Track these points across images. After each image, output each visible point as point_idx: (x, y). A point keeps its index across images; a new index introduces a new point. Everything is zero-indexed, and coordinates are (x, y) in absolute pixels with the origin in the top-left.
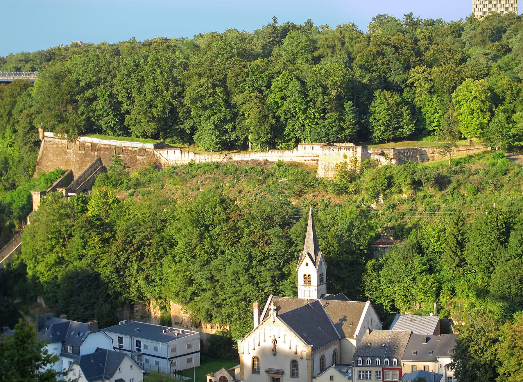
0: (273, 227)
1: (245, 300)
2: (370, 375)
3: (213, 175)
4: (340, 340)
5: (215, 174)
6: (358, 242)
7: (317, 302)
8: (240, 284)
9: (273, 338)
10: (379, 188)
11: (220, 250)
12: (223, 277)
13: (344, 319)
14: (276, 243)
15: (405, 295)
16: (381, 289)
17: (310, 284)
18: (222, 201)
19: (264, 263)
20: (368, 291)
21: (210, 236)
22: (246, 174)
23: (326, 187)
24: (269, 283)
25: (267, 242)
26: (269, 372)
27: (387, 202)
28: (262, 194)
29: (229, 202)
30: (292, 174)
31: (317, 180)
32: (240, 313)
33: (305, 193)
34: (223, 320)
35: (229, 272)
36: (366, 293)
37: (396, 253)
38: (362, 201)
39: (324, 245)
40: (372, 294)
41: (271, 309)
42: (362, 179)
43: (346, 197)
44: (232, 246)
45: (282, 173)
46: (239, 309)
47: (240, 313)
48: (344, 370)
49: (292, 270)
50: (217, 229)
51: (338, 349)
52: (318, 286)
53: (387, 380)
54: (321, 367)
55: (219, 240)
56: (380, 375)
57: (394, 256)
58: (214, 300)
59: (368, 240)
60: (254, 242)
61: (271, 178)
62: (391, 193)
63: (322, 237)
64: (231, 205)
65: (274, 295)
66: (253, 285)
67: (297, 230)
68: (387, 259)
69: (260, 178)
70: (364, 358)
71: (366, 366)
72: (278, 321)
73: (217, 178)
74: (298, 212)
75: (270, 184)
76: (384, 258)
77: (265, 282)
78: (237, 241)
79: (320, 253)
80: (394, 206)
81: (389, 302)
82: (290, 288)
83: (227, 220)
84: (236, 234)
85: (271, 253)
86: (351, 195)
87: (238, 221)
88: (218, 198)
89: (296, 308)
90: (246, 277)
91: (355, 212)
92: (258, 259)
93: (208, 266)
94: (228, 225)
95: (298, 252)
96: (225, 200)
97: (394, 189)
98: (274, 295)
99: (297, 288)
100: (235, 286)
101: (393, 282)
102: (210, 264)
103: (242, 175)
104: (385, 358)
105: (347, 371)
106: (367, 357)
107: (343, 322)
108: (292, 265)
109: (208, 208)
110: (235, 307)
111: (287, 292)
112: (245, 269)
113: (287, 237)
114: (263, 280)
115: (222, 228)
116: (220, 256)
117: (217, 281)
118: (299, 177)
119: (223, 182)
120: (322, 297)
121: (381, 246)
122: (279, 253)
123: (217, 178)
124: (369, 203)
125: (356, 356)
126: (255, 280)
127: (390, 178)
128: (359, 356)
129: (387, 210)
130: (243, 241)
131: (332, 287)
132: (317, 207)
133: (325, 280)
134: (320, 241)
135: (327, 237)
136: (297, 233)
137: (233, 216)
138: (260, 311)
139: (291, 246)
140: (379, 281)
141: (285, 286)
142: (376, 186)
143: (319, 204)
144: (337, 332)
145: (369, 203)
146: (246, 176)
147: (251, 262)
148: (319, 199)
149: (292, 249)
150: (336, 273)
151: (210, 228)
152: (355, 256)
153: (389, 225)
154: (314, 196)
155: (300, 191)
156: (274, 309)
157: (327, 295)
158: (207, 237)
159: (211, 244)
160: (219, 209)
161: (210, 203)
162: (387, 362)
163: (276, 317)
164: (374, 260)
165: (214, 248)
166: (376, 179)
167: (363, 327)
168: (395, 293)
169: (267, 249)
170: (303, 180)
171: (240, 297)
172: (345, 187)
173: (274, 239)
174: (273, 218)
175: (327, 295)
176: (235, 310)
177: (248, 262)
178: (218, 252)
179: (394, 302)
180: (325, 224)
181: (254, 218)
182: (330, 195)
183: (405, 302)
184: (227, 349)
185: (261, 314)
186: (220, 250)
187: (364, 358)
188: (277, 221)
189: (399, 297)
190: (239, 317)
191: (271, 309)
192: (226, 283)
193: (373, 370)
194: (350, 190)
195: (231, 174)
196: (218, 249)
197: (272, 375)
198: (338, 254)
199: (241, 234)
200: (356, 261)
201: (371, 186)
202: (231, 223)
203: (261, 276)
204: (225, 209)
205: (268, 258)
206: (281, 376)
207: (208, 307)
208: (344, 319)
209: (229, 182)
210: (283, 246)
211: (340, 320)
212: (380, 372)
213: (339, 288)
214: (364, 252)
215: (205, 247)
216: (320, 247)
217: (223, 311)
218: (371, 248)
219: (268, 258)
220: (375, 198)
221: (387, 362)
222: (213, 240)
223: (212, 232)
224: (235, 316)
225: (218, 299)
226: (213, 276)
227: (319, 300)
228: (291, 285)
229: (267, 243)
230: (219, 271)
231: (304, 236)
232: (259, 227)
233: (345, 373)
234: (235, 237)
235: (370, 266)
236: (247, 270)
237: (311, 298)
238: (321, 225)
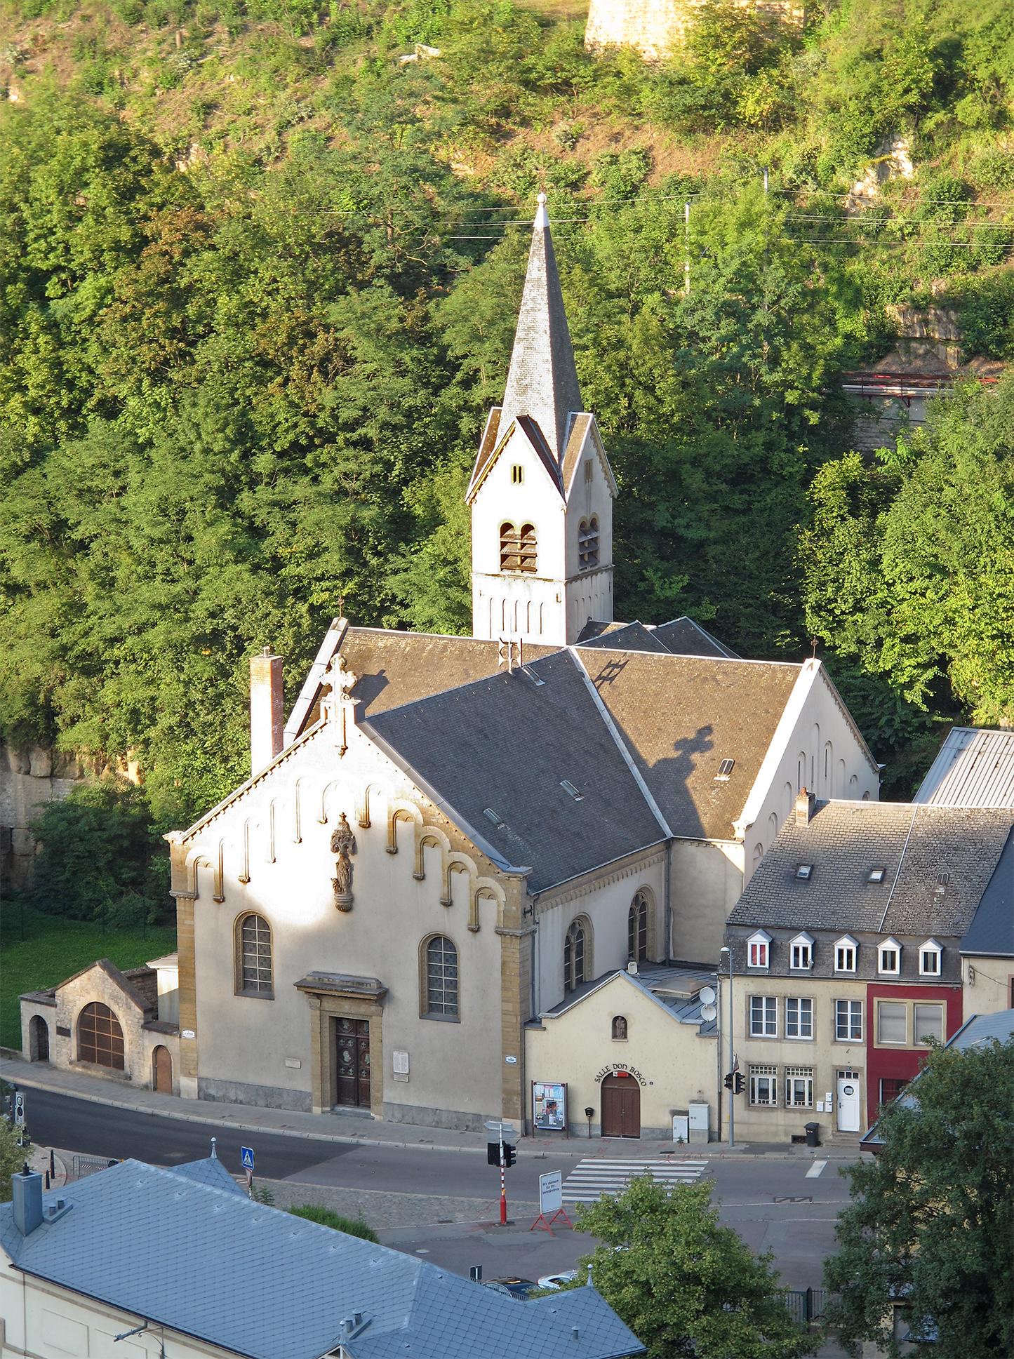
0: (362, 285)
1: (215, 638)
2: (806, 1017)
3: (76, 23)
4: (669, 844)
5: (86, 19)
6: (772, 370)
7: (563, 657)
8: (191, 562)
9: (334, 825)
10: (893, 102)
11: (97, 394)
12: (112, 527)
13: (700, 741)
14: (370, 367)
15: (1001, 635)
16: (883, 604)
18: (114, 155)
19: (309, 460)
20: (818, 609)
21: (51, 327)
22: (238, 21)
23: (628, 91)
24: (333, 562)
25: (327, 358)
26: (315, 989)
27: (932, 172)
28: (312, 125)
29: (144, 159)
30: (465, 28)
31: (588, 58)
32: (190, 705)
33: (525, 122)
34: (106, 737)
35: (140, 502)
36: (812, 622)
37: (967, 427)
38: (808, 166)
39: (607, 381)
40: (837, 625)
41: (329, 688)
42: (811, 55)
43: (723, 144)
44: (158, 376)
45: (414, 17)
46: (187, 684)
47: (190, 705)
48: (681, 990)
49: (445, 502)
50: (87, 290)
51: (659, 891)
52: (570, 580)
53: (888, 1043)
54: (567, 971)
55: (94, 349)
56: (856, 1019)
57: (950, 444)
58: (65, 638)
59: (830, 357)
60: (264, 362)
61: (361, 44)
62: (954, 129)
63: (596, 342)
64: (157, 176)
65: (355, 621)
66: (256, 568)
67: (473, 306)
68: (919, 454)
69: (307, 42)
70: (779, 932)
73: (93, 42)
74: (488, 216)
75: (353, 71)
76: (902, 450)
77: (313, 554)
78: (183, 355)
79: (585, 419)
80: (968, 192)
81: (924, 666)
82: (434, 587)
83: (134, 249)
84: (176, 321)
85: (346, 414)
86: (753, 137)
87: (186, 253)
88: (95, 137)
89: (456, 684)
90: (224, 528)
91: (764, 222)
92: (282, 444)
93: (36, 472)
94: (141, 276)
95: (477, 412)
96: (128, 148)
97: (969, 108)
98: (355, 621)
99: (466, 589)
100: (167, 572)
101: (943, 571)
102: (48, 467)
103: (217, 27)
104: (882, 936)
105: (697, 998)
106: (796, 930)
107: (695, 757)
108: (443, 480)
109: (43, 186)
110: (168, 676)
111: (421, 609)
112: (219, 491)
113: (424, 339)
114: (301, 544)
115: (110, 291)
116: (96, 424)
117: (82, 546)
118: (501, 42)
119: (125, 59)
120: (587, 633)
121: (897, 390)
122: (383, 413)
123: (93, 42)
124: (841, 178)
125: (739, 924)
126: (267, 546)
127: (951, 51)
128: (755, 927)
129: (931, 211)
130: (209, 352)
131: (642, 586)
132: (583, 194)
134: (585, 361)
135: (620, 343)
136: (475, 319)
137: (164, 229)
138: (285, 696)
139: (445, 383)
140: (875, 563)
141: (411, 576)
142: (877, 90)
143: (595, 177)
144: (653, 804)
145: (841, 178)
146: (237, 31)
147: (246, 456)
148: (593, 151)
149: (451, 396)
150: (661, 519)
151: (52, 289)
152: (759, 438)
153: (940, 285)
154: (573, 139)
155: (505, 112)
156: (344, 689)
157: (615, 626)
158: (34, 328)
159: (58, 363)
160: (96, 192)
161: (54, 163)
163: (353, 729)
164: (853, 460)
165: (71, 385)
166: (877, 55)
167: (784, 785)
168: (950, 622)
169: (328, 397)
170: (519, 56)
171: (192, 627)
172: (726, 95)
173: (363, 348)
174: (360, 242)
175: (615, 626)
176: (169, 691)
177: (234, 456)
178: (91, 403)
179: (944, 669)
180: (613, 276)
181: (262, 241)
182: (653, 135)
183: (1000, 669)
184: (127, 875)
185: (289, 711)
186: (97, 394)
187: (780, 936)
188: (379, 257)
189: (973, 642)
190: (184, 723)
191: (329, 688)
192: (125, 559)
193: (823, 993)
194: (749, 107)
195: (163, 22)
196: (88, 393)
197: (329, 1005)
198: (676, 429)
199: (199, 321)
200: (764, 461)
201: (854, 89)
202: (152, 264)
203: (294, 524)
204: (127, 194)
205: (331, 439)
206: (373, 1008)
207: (37, 669)
208: (700, 741)
209: (152, 62)
210: (404, 384)
211: (678, 745)
212: (856, 1005)
213: (674, 591)
214: (805, 420)
215: (29, 382)
216: (587, 392)
217: (108, 694)
218: (842, 398)
219: (331, 439)
220: (870, 152)
221: (889, 960)
222: (62, 345)
223: (59, 307)
224: (166, 720)
225: (86, 634)
226: (60, 525)
227: (573, 649)
228: (441, 574)
229: (325, 368)
230: (91, 497)
231: (508, 340)
232: (290, 286)
233: (686, 1007)
234: (172, 333)
235: (832, 487)
236: (226, 495)
237: (531, 639)
238: (592, 282)
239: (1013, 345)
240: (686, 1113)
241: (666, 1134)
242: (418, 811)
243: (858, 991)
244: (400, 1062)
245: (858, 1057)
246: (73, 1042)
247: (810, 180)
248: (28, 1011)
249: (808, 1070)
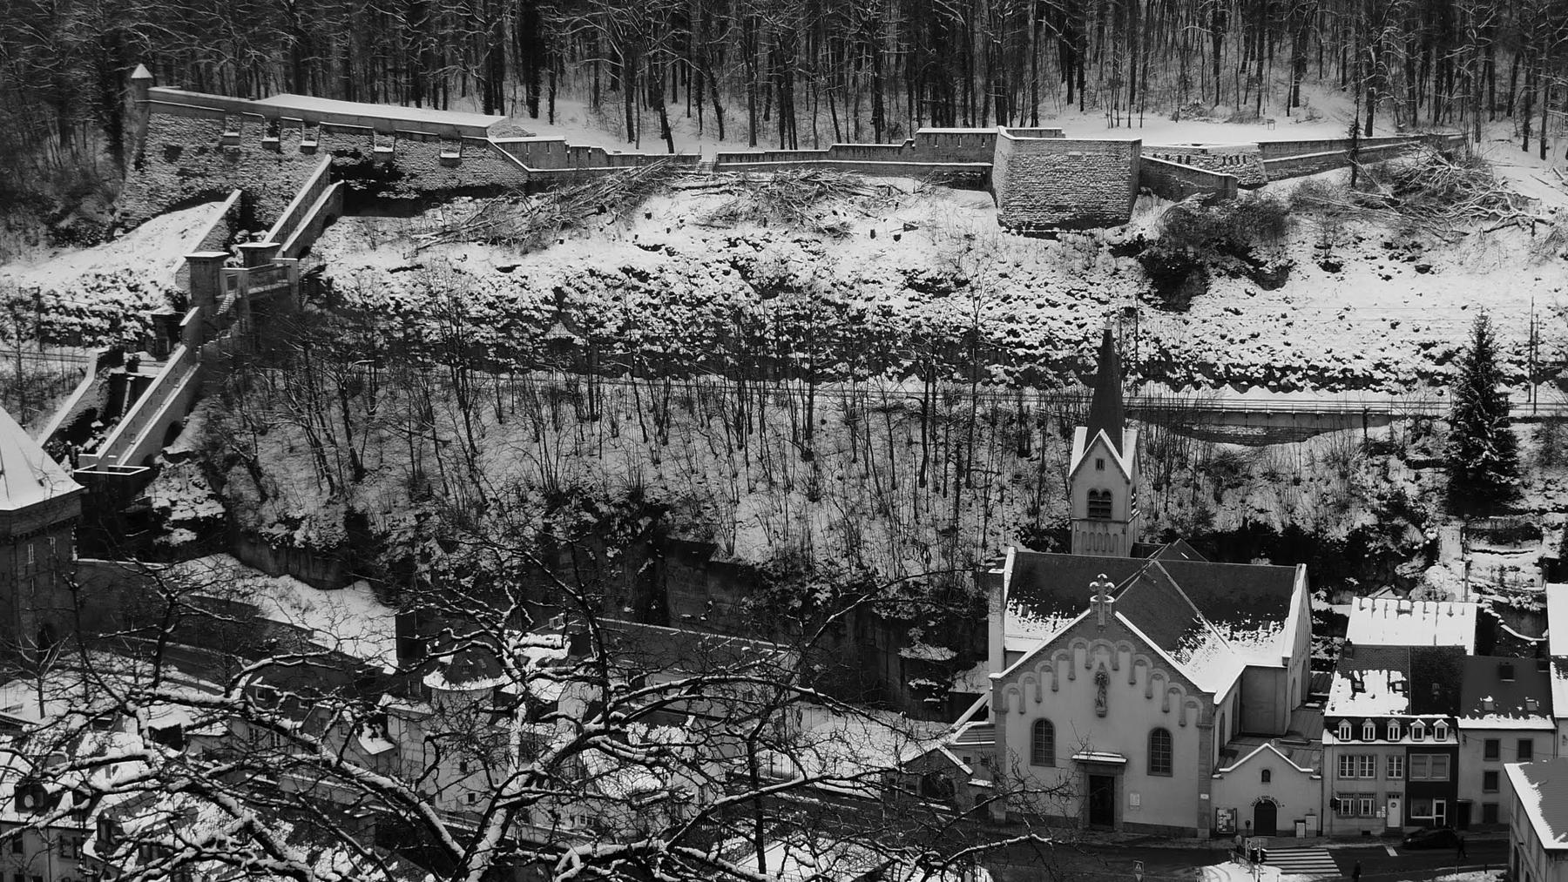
2: (1343, 766)
56: (1399, 766)
240: (1304, 821)
241: (1293, 833)
244: (1134, 799)
245: (1401, 787)
247: (1140, 331)
249: (1371, 795)
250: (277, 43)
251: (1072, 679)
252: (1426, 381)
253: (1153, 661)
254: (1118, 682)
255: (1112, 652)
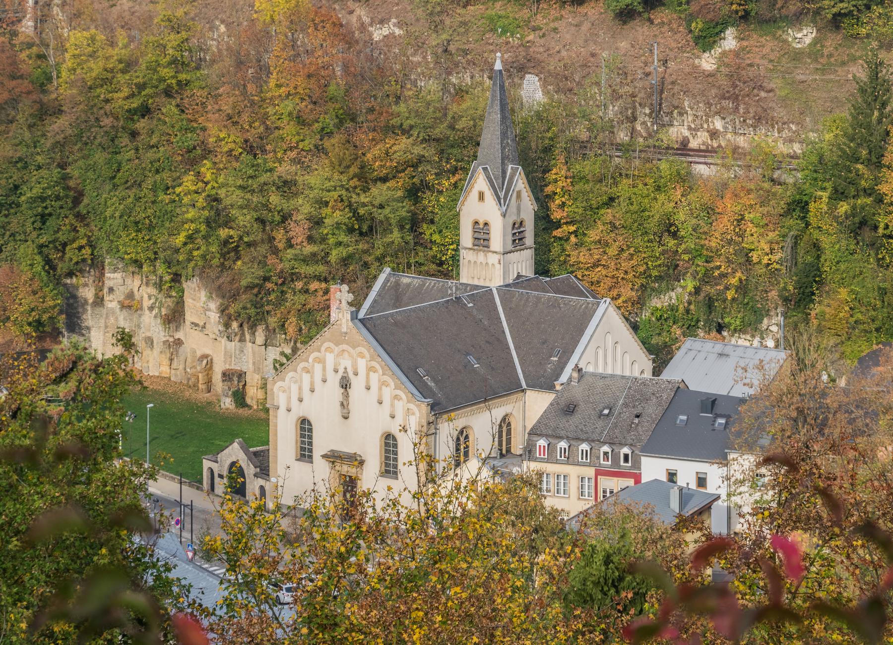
17: (488, 247)
26: (333, 457)
71: (557, 462)
72: (361, 335)
133: (529, 240)
162: (606, 454)
187: (553, 441)
193: (573, 472)
239: (891, 70)
242: (257, 334)
243: (590, 472)
246: (225, 481)
248: (206, 464)
250: (306, 277)
251: (346, 418)
252: (326, 138)
253: (382, 368)
254: (357, 384)
255: (352, 357)
